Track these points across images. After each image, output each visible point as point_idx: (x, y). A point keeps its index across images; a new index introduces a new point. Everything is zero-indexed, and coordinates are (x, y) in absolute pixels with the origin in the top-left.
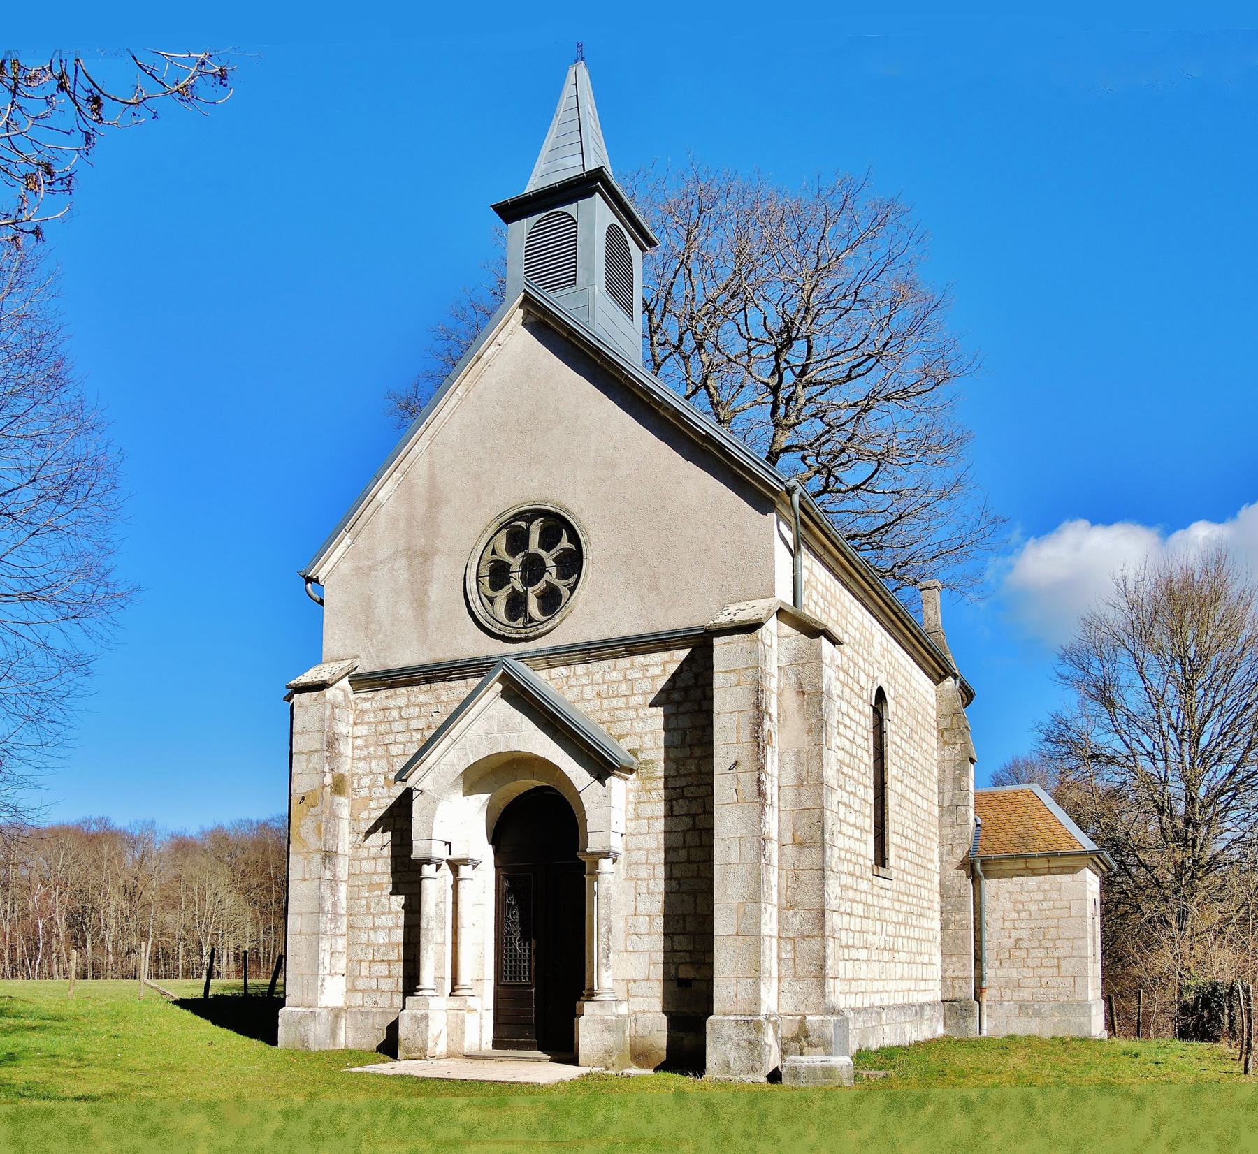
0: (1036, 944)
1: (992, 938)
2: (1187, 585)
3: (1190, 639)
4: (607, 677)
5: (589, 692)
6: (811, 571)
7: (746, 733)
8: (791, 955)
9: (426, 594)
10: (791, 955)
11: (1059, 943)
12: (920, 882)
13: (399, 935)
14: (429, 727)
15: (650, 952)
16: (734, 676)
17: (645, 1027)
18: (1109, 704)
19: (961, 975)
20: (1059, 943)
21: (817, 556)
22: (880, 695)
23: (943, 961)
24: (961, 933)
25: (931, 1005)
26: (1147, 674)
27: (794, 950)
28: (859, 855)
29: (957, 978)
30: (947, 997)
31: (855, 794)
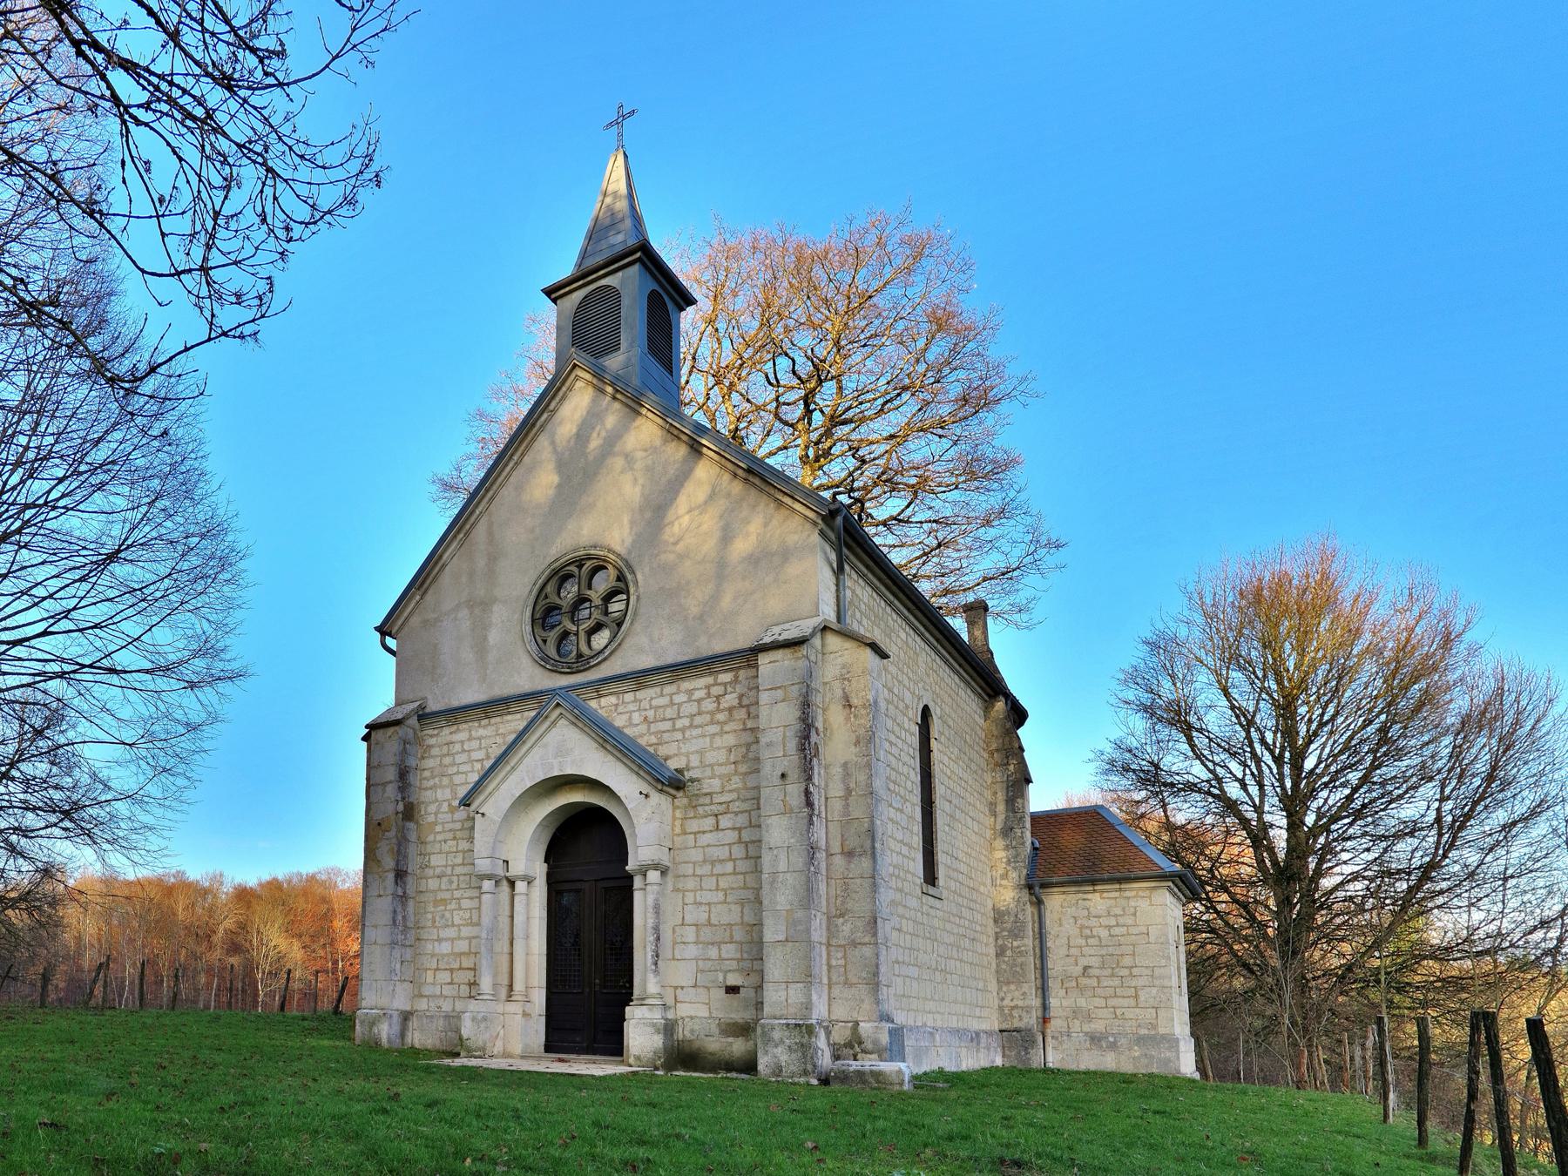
0: (1108, 972)
1: (1056, 964)
2: (1282, 582)
3: (1288, 651)
4: (654, 703)
5: (636, 718)
6: (853, 592)
7: (792, 745)
8: (842, 962)
9: (485, 638)
10: (842, 962)
11: (1135, 972)
12: (972, 905)
13: (700, 683)
14: (488, 757)
15: (697, 959)
16: (779, 694)
17: (692, 1031)
18: (1188, 730)
19: (1020, 1003)
20: (1135, 972)
21: (862, 576)
22: (926, 712)
23: (1000, 988)
24: (1020, 960)
25: (989, 1033)
26: (1234, 693)
27: (845, 957)
28: (908, 871)
29: (1016, 1007)
30: (1004, 1026)
31: (902, 811)
